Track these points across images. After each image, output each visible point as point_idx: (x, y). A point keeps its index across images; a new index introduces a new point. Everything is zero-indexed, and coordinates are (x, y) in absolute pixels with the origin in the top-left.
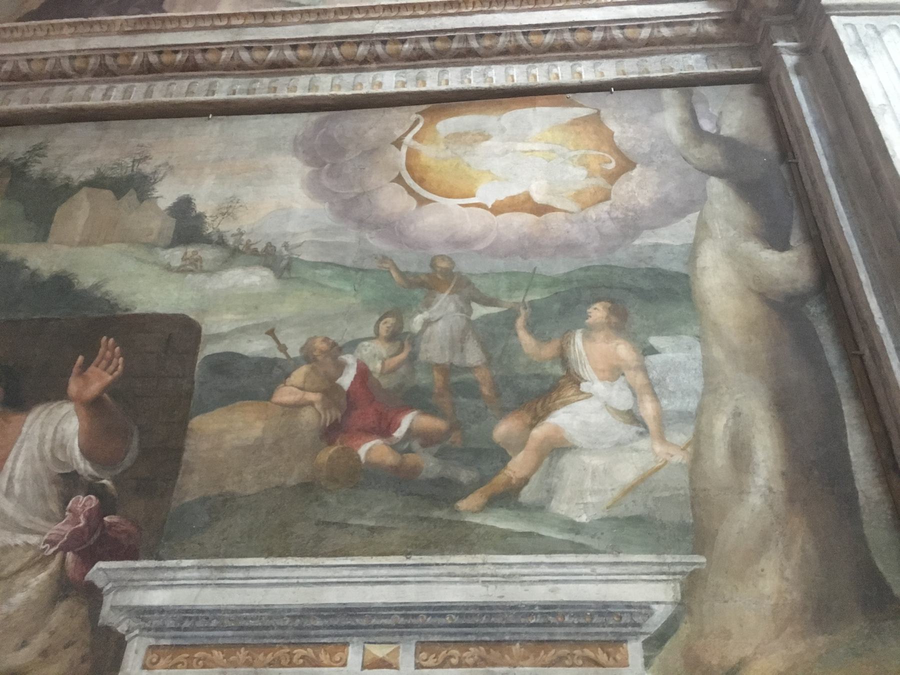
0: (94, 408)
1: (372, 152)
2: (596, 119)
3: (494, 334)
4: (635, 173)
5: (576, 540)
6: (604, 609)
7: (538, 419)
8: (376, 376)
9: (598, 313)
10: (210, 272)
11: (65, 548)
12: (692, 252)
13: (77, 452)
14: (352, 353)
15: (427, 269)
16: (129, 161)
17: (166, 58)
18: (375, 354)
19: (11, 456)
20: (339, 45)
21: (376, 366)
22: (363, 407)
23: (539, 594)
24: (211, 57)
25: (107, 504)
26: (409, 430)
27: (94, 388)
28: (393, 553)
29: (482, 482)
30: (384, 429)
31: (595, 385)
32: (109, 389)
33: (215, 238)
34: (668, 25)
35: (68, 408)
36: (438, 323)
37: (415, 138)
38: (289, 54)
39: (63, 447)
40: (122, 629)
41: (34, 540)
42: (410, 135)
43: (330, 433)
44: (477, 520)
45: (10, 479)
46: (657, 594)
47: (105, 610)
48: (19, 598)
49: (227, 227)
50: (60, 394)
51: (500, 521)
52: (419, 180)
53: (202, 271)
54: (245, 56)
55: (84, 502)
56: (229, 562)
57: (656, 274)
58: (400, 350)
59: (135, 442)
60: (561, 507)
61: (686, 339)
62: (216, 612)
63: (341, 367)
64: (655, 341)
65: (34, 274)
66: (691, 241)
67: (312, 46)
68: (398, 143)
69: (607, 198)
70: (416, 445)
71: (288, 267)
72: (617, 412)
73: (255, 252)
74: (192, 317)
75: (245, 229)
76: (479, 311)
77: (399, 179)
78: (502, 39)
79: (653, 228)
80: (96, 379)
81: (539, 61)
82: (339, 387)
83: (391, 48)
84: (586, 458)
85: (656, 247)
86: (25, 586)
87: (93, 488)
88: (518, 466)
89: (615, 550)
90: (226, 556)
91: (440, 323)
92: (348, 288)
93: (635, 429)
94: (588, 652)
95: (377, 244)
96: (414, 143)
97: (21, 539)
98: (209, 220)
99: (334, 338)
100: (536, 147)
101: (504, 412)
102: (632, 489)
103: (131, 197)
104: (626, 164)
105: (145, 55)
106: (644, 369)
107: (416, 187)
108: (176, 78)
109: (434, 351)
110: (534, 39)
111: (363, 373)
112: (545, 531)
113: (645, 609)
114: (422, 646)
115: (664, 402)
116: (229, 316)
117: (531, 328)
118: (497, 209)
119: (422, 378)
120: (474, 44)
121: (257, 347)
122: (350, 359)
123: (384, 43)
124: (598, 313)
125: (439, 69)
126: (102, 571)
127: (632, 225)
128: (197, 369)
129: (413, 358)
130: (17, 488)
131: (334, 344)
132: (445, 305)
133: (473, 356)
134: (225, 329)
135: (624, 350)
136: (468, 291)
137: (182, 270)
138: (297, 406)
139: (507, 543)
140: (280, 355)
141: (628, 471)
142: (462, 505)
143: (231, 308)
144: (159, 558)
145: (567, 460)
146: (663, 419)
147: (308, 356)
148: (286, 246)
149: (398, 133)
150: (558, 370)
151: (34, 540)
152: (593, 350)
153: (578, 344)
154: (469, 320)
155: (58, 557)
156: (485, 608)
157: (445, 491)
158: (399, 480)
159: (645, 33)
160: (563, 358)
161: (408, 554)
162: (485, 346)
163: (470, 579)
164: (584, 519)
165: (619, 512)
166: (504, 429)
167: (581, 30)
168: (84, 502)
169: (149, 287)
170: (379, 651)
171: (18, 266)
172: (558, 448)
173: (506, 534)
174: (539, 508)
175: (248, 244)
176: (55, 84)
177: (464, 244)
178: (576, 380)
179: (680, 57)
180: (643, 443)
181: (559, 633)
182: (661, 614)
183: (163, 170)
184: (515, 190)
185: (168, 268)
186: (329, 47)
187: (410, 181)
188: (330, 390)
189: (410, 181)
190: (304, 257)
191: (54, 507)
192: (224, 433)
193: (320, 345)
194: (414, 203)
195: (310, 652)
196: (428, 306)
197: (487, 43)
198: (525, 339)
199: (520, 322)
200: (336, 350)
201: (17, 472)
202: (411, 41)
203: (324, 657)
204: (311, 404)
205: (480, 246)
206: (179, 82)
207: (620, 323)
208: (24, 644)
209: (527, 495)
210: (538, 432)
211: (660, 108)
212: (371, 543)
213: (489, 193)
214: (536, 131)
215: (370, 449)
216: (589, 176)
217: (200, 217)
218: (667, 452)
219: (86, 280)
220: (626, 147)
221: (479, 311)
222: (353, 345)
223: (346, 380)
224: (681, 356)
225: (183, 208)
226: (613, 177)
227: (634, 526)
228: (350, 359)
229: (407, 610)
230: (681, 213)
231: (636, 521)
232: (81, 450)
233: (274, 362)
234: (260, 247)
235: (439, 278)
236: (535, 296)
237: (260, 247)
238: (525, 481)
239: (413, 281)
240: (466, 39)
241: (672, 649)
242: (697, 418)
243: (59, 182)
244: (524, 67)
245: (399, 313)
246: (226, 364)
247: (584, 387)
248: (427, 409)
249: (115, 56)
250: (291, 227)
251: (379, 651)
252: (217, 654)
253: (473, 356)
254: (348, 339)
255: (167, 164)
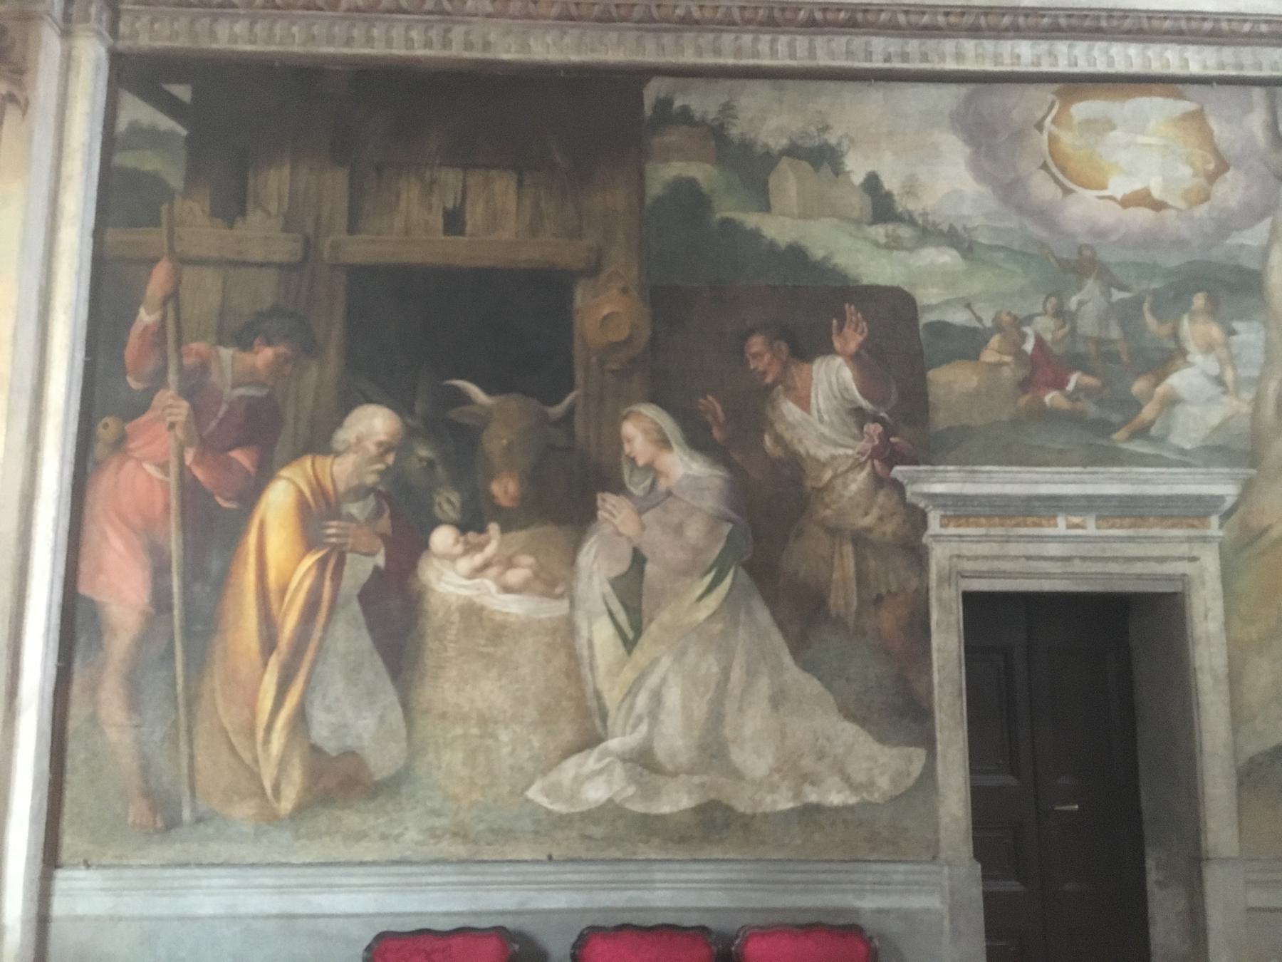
0: (855, 359)
1: (1019, 136)
2: (1198, 117)
3: (1128, 314)
4: (1229, 175)
5: (1184, 459)
6: (1199, 499)
7: (1160, 379)
8: (1049, 344)
9: (1199, 300)
10: (911, 250)
11: (871, 457)
12: (1265, 253)
13: (857, 394)
14: (1029, 325)
15: (1075, 257)
16: (813, 129)
17: (830, 16)
18: (1045, 326)
19: (813, 395)
20: (986, 14)
21: (1048, 337)
22: (1044, 368)
23: (1163, 490)
24: (871, 17)
25: (888, 432)
26: (1076, 386)
27: (852, 346)
28: (1076, 465)
29: (1126, 422)
30: (1060, 384)
31: (1196, 357)
32: (862, 346)
33: (907, 217)
34: (1267, 22)
35: (839, 360)
36: (1088, 300)
37: (1054, 121)
38: (941, 19)
39: (847, 389)
40: (922, 505)
41: (850, 452)
42: (1049, 119)
43: (1024, 385)
44: (1125, 446)
45: (819, 411)
46: (1227, 490)
47: (908, 494)
48: (854, 487)
49: (912, 205)
50: (829, 350)
51: (1138, 447)
52: (1060, 167)
53: (903, 248)
54: (902, 19)
55: (874, 429)
56: (977, 468)
57: (1240, 270)
58: (1063, 326)
59: (894, 390)
60: (1176, 439)
61: (1256, 324)
62: (975, 497)
63: (1024, 337)
64: (1237, 325)
65: (772, 243)
66: (1265, 242)
67: (963, 14)
68: (1040, 126)
69: (1207, 198)
70: (1081, 396)
71: (970, 249)
72: (1208, 376)
73: (941, 233)
74: (906, 289)
75: (928, 210)
76: (1117, 295)
77: (1045, 166)
78: (1128, 21)
79: (1238, 230)
80: (852, 338)
81: (1153, 41)
82: (1024, 352)
83: (1032, 21)
84: (1195, 410)
85: (1242, 246)
86: (855, 480)
87: (876, 419)
88: (1148, 412)
89: (1206, 465)
90: (974, 464)
91: (1090, 304)
92: (1019, 270)
93: (1220, 389)
94: (1191, 521)
95: (1039, 232)
96: (1053, 128)
97: (841, 451)
98: (897, 198)
99: (1014, 312)
100: (1154, 141)
101: (1138, 375)
102: (1217, 429)
103: (826, 170)
104: (1223, 166)
105: (812, 11)
106: (1227, 345)
107: (1060, 176)
108: (836, 34)
109: (1088, 325)
110: (1155, 23)
111: (1040, 342)
112: (1165, 454)
113: (1221, 498)
114: (1098, 518)
115: (1240, 371)
116: (935, 291)
117: (1154, 312)
118: (1126, 202)
119: (1081, 348)
120: (1104, 23)
121: (959, 317)
122: (1028, 330)
123: (1027, 16)
124: (1199, 300)
125: (1068, 42)
126: (899, 471)
127: (1225, 226)
128: (921, 333)
129: (1073, 331)
130: (826, 418)
131: (1015, 318)
132: (1091, 288)
133: (1115, 332)
134: (934, 301)
135: (1215, 332)
136: (1109, 280)
137: (888, 247)
138: (999, 365)
139: (1142, 460)
140: (978, 325)
141: (1215, 417)
142: (1115, 436)
143: (935, 280)
144: (932, 464)
145: (1178, 409)
146: (1237, 381)
147: (998, 327)
148: (965, 228)
149: (1039, 115)
150: (1171, 345)
151: (850, 452)
152: (1196, 330)
153: (1186, 324)
154: (1109, 302)
155: (869, 462)
156: (1133, 498)
157: (1106, 428)
158: (1074, 419)
159: (1247, 27)
160: (1175, 335)
161: (1084, 466)
162: (1122, 325)
163: (1122, 481)
164: (1188, 446)
165: (1209, 443)
166: (1139, 386)
167: (1195, 19)
168: (874, 429)
169: (871, 263)
170: (1076, 520)
171: (756, 235)
172: (1172, 401)
173: (1142, 456)
174: (1161, 440)
175: (935, 225)
176: (722, 31)
177: (1101, 234)
178: (1183, 353)
179: (1269, 50)
180: (1225, 399)
181: (1175, 512)
182: (1229, 502)
183: (845, 143)
184: (1138, 186)
185: (877, 244)
186: (978, 16)
187: (1054, 170)
188: (1019, 353)
189: (1054, 170)
190: (982, 240)
191: (855, 431)
192: (952, 382)
193: (1006, 318)
194: (1059, 193)
195: (1035, 519)
196: (1080, 289)
197: (1115, 23)
198: (1150, 320)
199: (1146, 306)
200: (1019, 323)
201: (822, 407)
202: (1050, 16)
203: (1044, 522)
204: (1007, 364)
205: (1114, 238)
206: (837, 38)
207: (1213, 311)
208: (866, 514)
209: (1153, 431)
210: (1160, 390)
211: (1248, 109)
212: (1061, 458)
213: (1119, 186)
214: (1152, 125)
215: (1051, 398)
216: (1195, 175)
217: (889, 195)
218: (1236, 406)
219: (818, 253)
220: (1222, 146)
221: (1117, 295)
222: (1029, 320)
223: (1029, 346)
224: (1252, 337)
225: (872, 183)
226: (1212, 178)
227: (1218, 451)
228: (1028, 330)
229: (1089, 498)
230: (1261, 217)
231: (1219, 448)
232: (860, 393)
233: (974, 330)
234: (945, 228)
235: (1082, 264)
236: (1155, 285)
237: (945, 228)
238: (1152, 422)
239: (1065, 266)
240: (1098, 18)
241: (1235, 518)
242: (1259, 382)
243: (759, 150)
244: (1140, 46)
245: (1060, 294)
246: (941, 329)
247: (1189, 358)
248: (1087, 371)
249: (783, 10)
250: (966, 210)
251: (1076, 520)
252: (983, 520)
253: (1115, 332)
254: (1025, 314)
255: (846, 135)
